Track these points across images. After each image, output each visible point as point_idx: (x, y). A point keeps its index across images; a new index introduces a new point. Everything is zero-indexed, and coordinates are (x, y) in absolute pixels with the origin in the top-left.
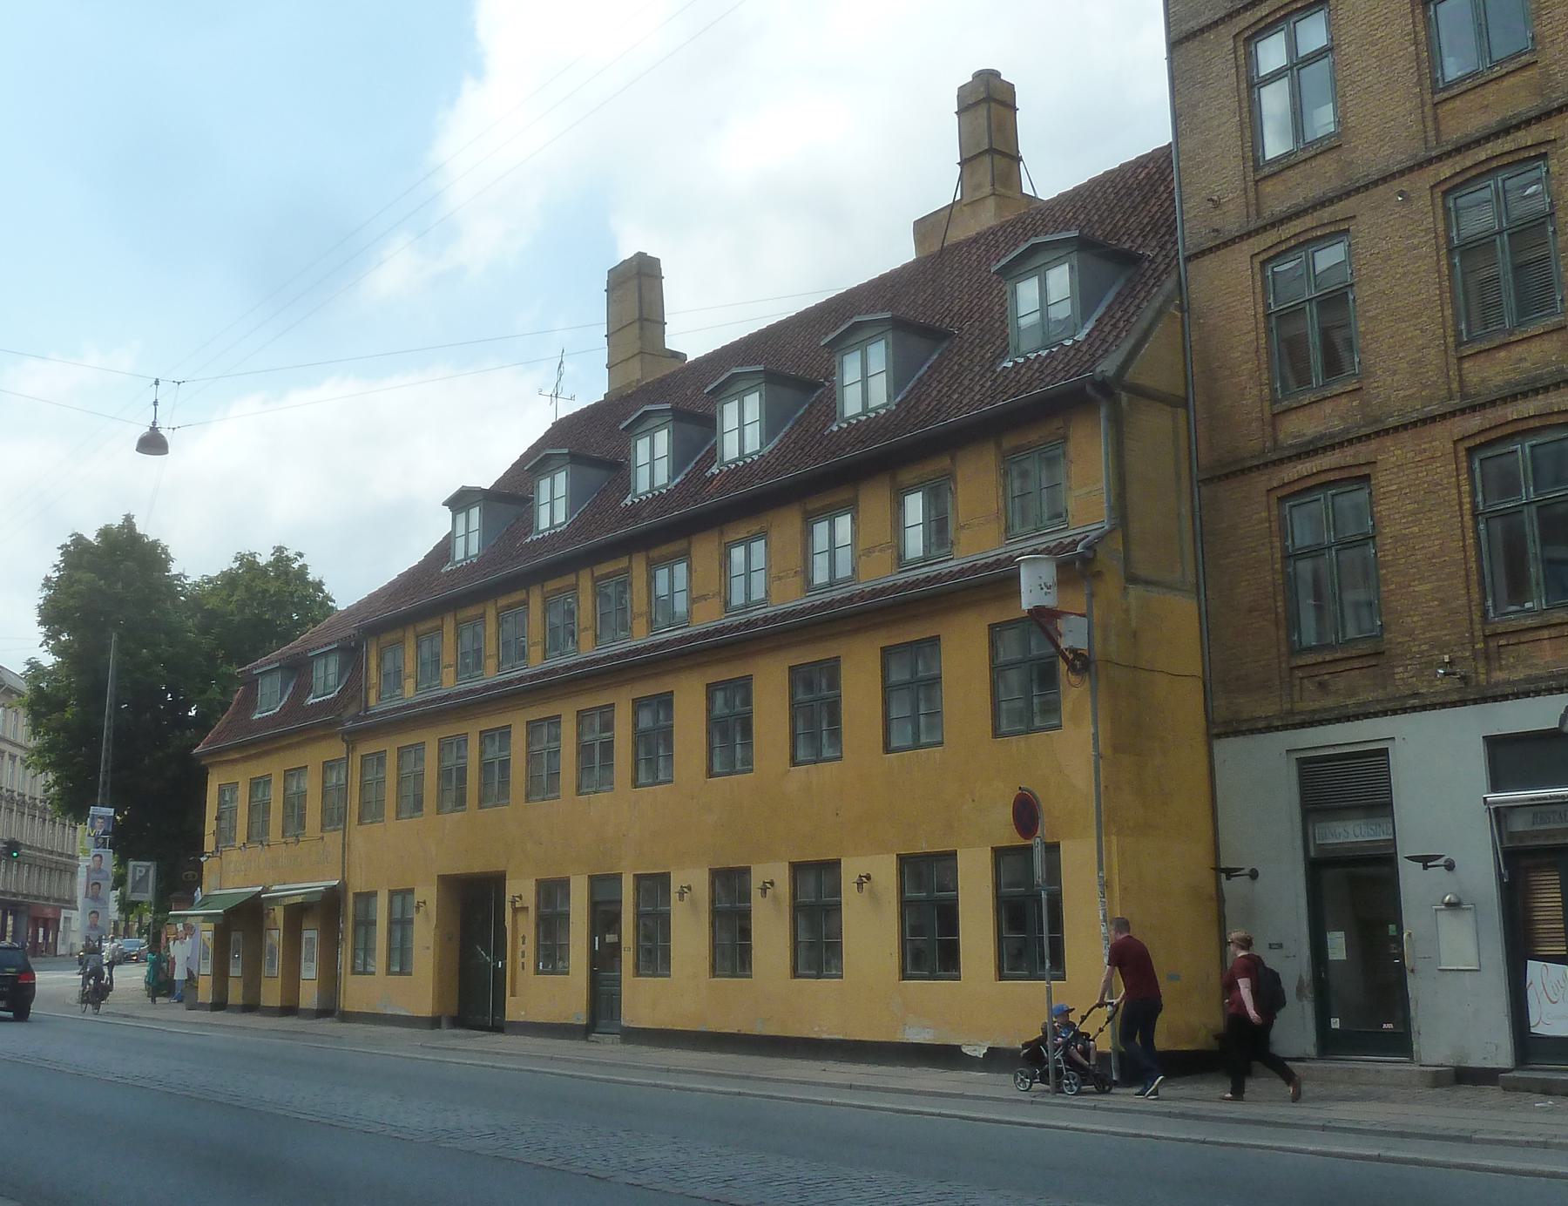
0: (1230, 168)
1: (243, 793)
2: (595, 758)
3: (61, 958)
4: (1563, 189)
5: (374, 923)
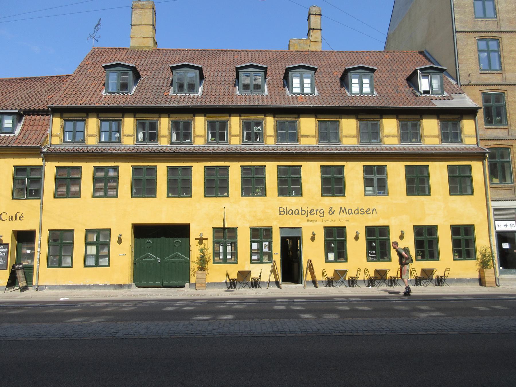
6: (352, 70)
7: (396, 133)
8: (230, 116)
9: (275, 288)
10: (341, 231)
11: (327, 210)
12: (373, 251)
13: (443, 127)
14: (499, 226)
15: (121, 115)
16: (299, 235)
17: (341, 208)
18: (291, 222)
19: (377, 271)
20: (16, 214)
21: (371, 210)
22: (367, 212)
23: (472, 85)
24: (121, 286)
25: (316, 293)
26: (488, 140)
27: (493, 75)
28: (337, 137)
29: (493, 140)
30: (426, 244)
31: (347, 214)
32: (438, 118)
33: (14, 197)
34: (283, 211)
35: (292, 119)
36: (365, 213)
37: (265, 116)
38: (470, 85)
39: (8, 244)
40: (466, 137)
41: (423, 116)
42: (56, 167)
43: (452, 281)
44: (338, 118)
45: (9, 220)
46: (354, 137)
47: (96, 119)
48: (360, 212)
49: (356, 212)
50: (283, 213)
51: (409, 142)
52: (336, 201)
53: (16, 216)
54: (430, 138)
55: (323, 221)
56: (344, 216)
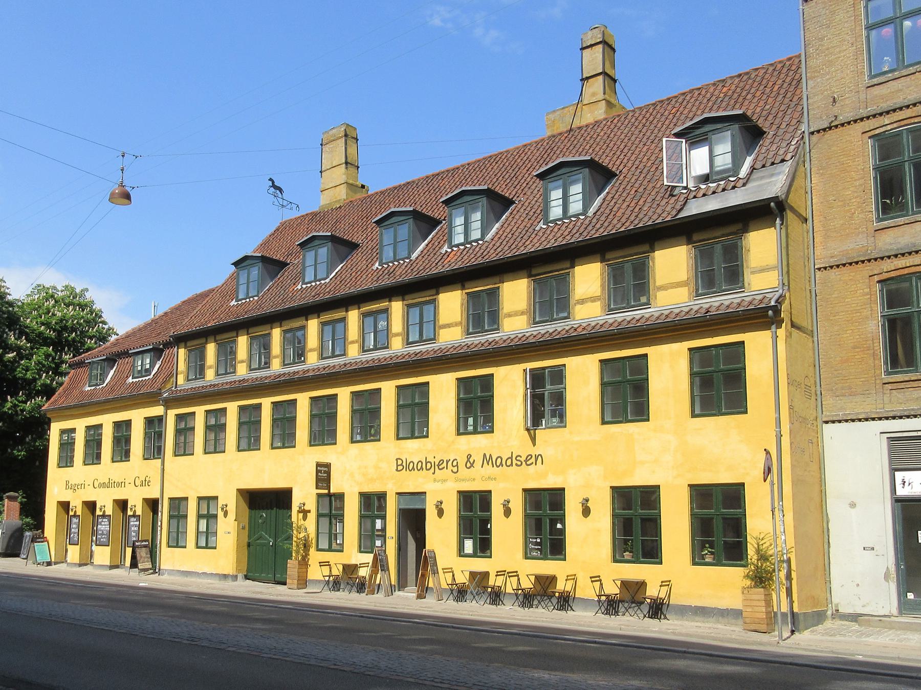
0: (847, 78)
1: (199, 424)
2: (216, 428)
3: (905, 595)
4: (115, 331)
5: (186, 517)
6: (549, 175)
7: (598, 292)
8: (347, 311)
9: (451, 603)
10: (485, 498)
11: (462, 461)
12: (536, 539)
13: (703, 257)
14: (906, 484)
15: (234, 334)
16: (424, 507)
17: (485, 455)
18: (413, 483)
19: (625, 585)
21: (534, 457)
22: (526, 461)
23: (842, 125)
24: (225, 577)
25: (355, 602)
26: (882, 258)
27: (908, 79)
28: (735, 276)
29: (896, 256)
30: (637, 526)
31: (493, 466)
32: (689, 241)
33: (401, 436)
34: (402, 465)
35: (428, 299)
36: (524, 463)
37: (390, 301)
38: (836, 127)
39: (79, 516)
40: (753, 273)
41: (656, 243)
42: (599, 360)
43: (684, 611)
44: (498, 281)
46: (522, 313)
47: (526, 280)
48: (515, 462)
49: (509, 462)
50: (401, 467)
51: (624, 308)
52: (478, 443)
53: (145, 481)
54: (669, 290)
55: (457, 480)
56: (489, 470)
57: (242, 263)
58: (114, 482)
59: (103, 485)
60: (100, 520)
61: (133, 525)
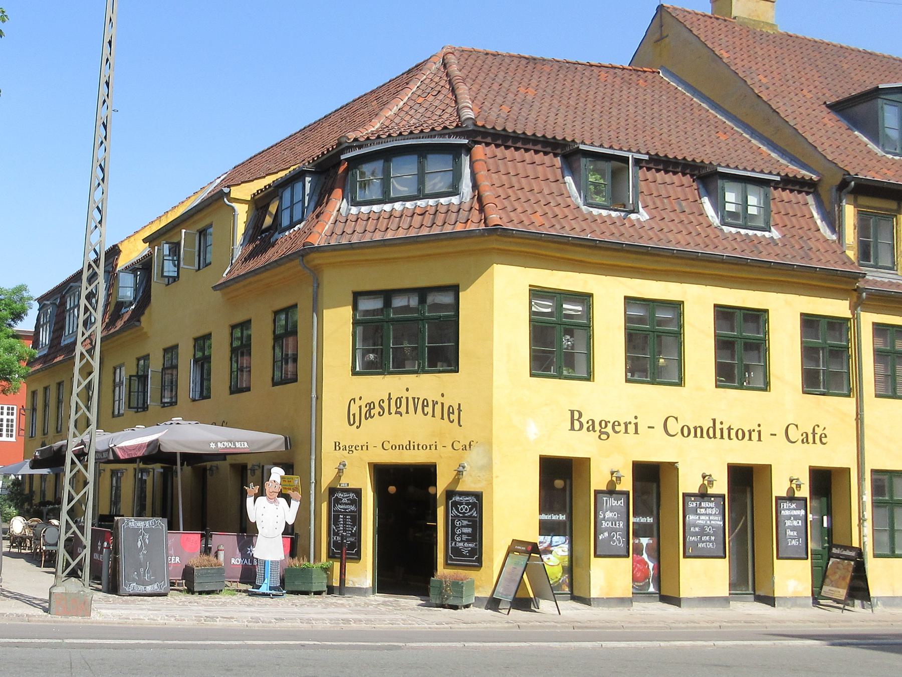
20: (470, 443)
45: (463, 450)
53: (814, 433)
57: (891, 93)
58: (729, 429)
59: (698, 432)
60: (692, 505)
61: (789, 517)
